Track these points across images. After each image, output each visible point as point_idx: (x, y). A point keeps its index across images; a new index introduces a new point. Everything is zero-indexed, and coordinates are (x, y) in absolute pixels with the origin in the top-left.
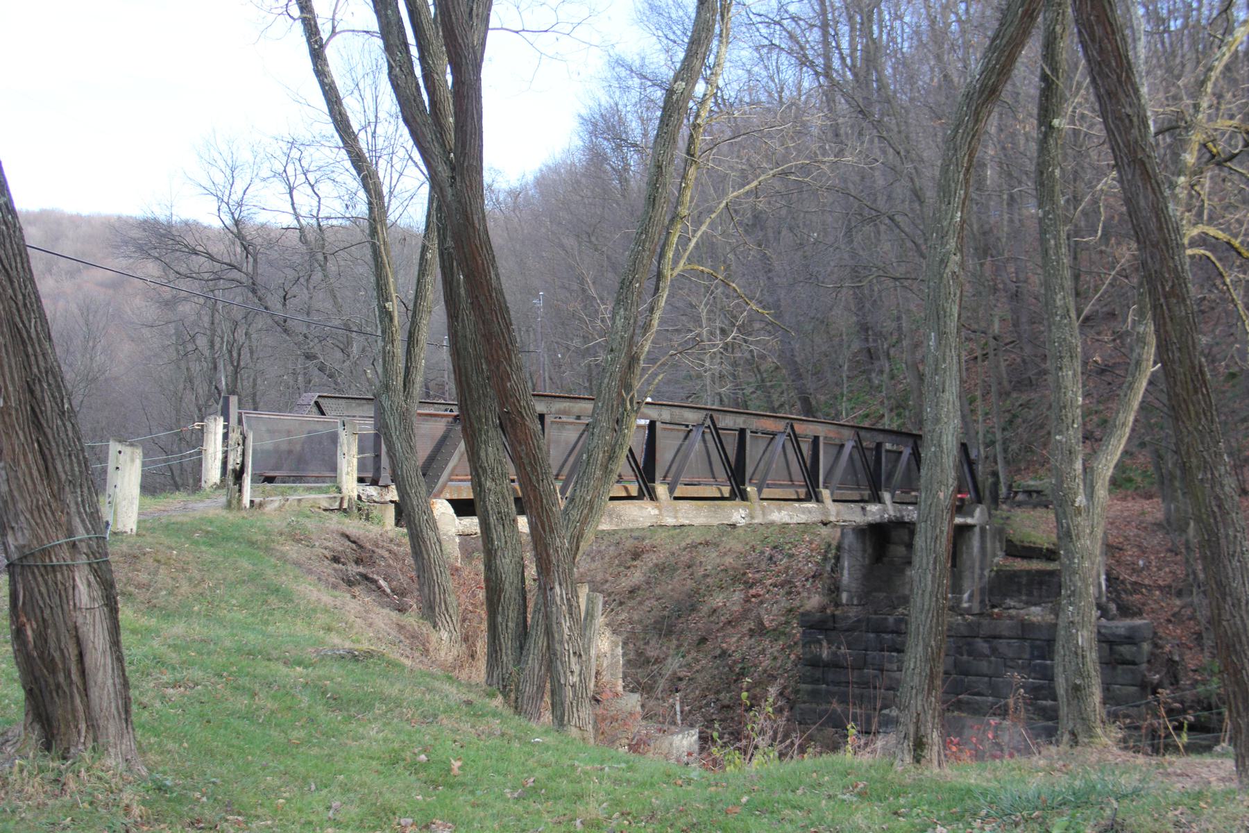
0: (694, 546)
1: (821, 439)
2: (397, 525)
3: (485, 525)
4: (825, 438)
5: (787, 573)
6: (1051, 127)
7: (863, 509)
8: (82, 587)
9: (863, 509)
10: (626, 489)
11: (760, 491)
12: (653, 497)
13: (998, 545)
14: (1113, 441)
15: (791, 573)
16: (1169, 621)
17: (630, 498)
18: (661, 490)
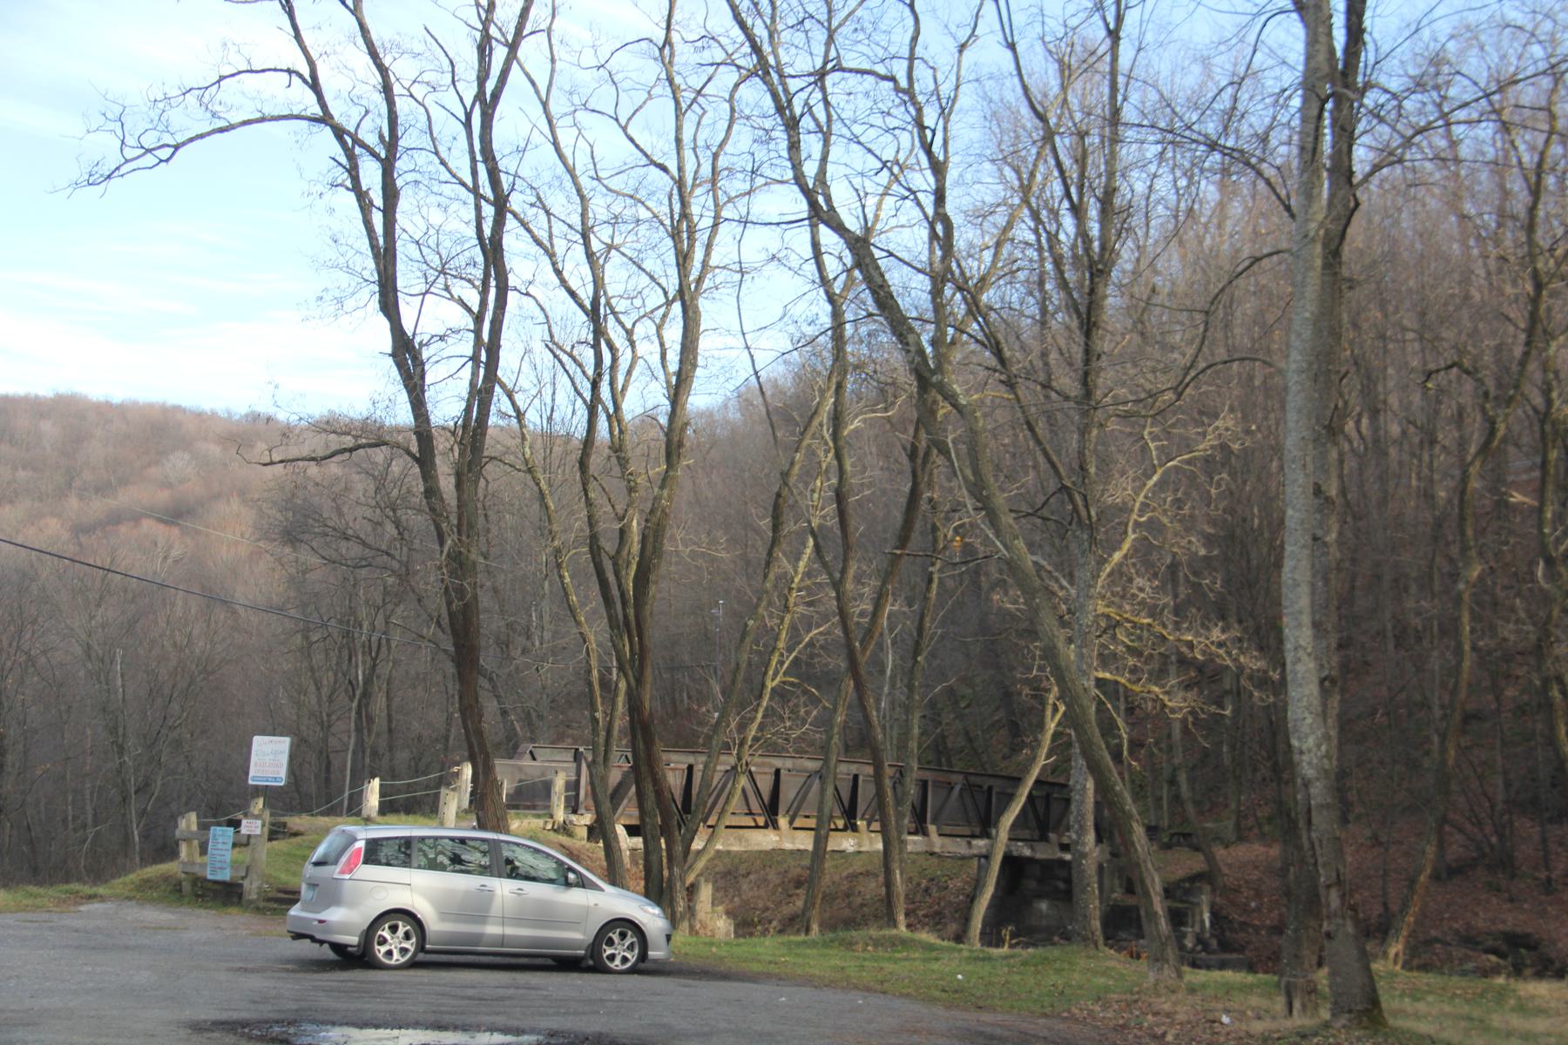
0: (853, 877)
1: (930, 783)
2: (588, 839)
3: (645, 842)
4: (934, 782)
5: (939, 904)
6: (916, 661)
7: (969, 843)
8: (1178, 731)
9: (969, 843)
10: (755, 821)
11: (869, 825)
12: (776, 826)
13: (1117, 882)
14: (1014, 805)
15: (942, 904)
16: (1269, 958)
17: (757, 827)
18: (783, 822)
